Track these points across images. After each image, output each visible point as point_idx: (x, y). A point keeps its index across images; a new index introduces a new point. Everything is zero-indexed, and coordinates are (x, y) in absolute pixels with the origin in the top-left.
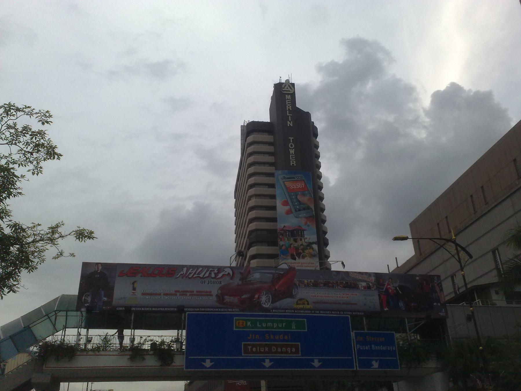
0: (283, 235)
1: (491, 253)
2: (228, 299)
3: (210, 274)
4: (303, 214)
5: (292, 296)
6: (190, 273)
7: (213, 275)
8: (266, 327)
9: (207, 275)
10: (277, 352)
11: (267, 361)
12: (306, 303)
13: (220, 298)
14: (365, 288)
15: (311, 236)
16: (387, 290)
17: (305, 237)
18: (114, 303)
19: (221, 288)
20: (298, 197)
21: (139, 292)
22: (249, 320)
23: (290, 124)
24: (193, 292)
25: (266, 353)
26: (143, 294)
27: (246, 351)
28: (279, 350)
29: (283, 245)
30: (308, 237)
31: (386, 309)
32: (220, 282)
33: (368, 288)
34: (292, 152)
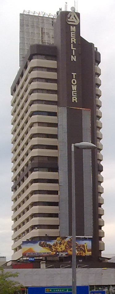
22: (51, 289)
23: (74, 58)
34: (74, 88)
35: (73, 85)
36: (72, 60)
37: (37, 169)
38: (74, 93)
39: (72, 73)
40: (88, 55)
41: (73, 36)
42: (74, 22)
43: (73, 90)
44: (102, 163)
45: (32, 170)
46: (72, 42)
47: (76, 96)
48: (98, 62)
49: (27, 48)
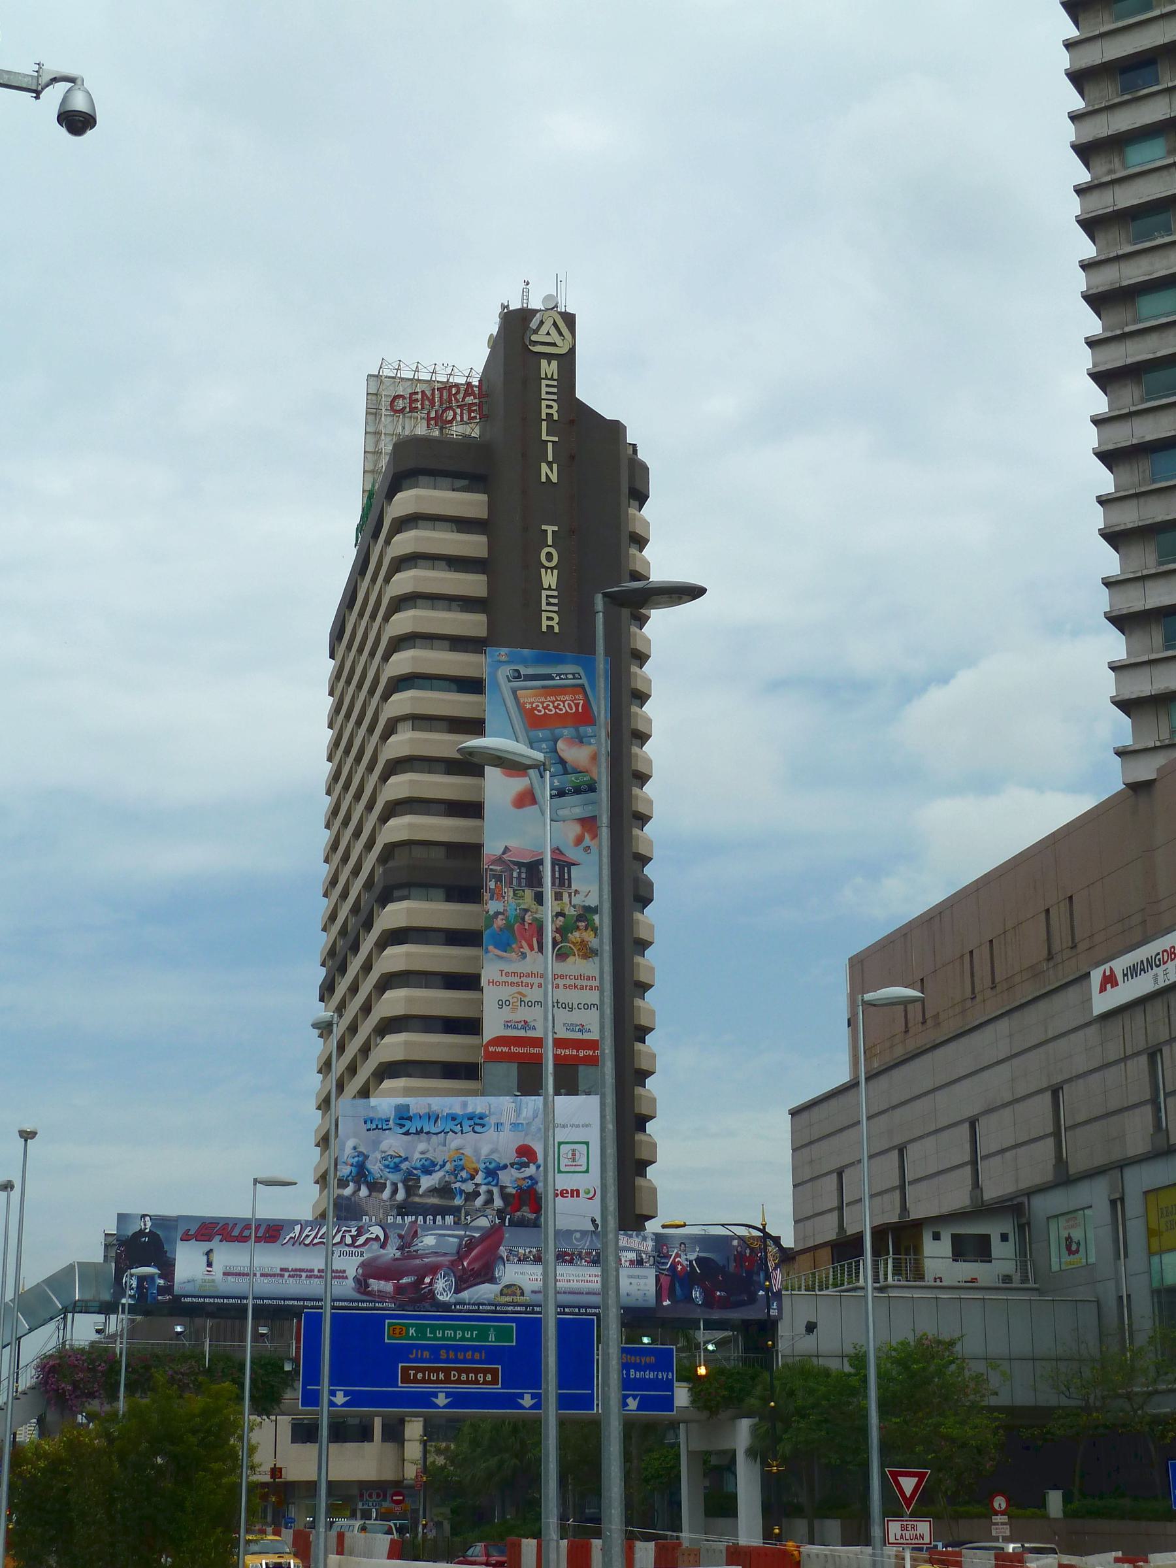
0: (498, 879)
1: (967, 1125)
2: (375, 1285)
3: (343, 1237)
4: (574, 807)
5: (492, 1280)
6: (308, 1236)
7: (348, 1240)
8: (443, 1338)
9: (337, 1239)
10: (459, 1381)
11: (442, 1396)
12: (518, 1292)
13: (361, 1284)
14: (632, 1262)
15: (590, 886)
16: (674, 1266)
17: (574, 887)
18: (177, 1289)
19: (363, 1265)
20: (560, 745)
21: (218, 1269)
23: (549, 473)
24: (312, 1271)
25: (441, 1382)
26: (225, 1274)
27: (406, 1379)
28: (464, 1377)
29: (497, 914)
30: (583, 889)
31: (667, 1303)
32: (362, 1255)
33: (640, 1262)
34: (549, 579)
35: (547, 568)
36: (543, 479)
37: (405, 892)
38: (548, 596)
39: (544, 527)
40: (603, 472)
41: (547, 393)
42: (554, 345)
43: (546, 586)
44: (649, 870)
45: (385, 899)
46: (544, 417)
47: (556, 609)
48: (640, 496)
49: (387, 447)
